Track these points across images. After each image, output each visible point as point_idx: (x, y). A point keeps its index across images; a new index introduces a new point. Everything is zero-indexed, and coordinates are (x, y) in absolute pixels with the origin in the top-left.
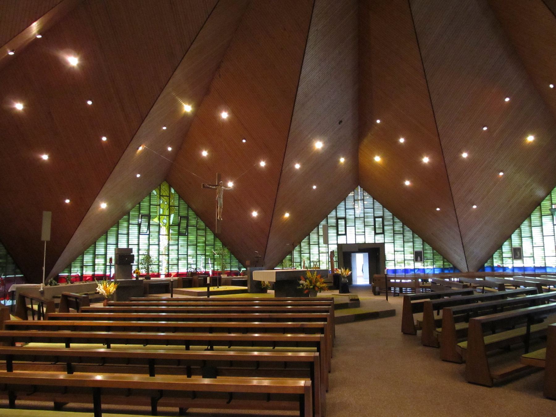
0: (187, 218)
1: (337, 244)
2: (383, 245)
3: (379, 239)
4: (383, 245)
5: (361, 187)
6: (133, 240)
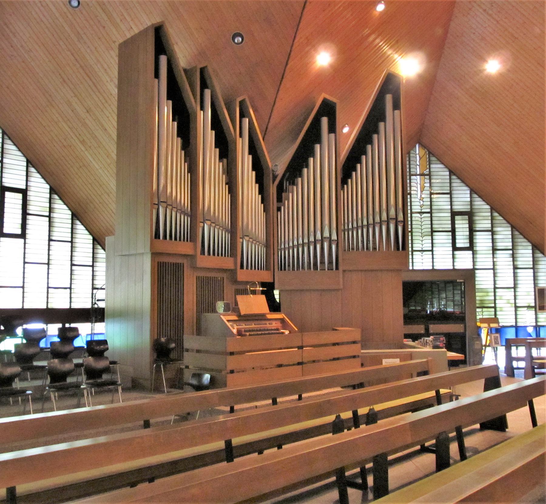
0: (470, 215)
1: (474, 269)
2: (469, 275)
3: (464, 261)
4: (469, 275)
5: (423, 146)
6: (484, 259)
